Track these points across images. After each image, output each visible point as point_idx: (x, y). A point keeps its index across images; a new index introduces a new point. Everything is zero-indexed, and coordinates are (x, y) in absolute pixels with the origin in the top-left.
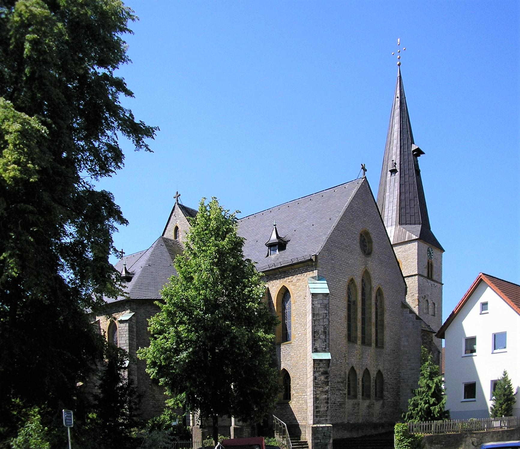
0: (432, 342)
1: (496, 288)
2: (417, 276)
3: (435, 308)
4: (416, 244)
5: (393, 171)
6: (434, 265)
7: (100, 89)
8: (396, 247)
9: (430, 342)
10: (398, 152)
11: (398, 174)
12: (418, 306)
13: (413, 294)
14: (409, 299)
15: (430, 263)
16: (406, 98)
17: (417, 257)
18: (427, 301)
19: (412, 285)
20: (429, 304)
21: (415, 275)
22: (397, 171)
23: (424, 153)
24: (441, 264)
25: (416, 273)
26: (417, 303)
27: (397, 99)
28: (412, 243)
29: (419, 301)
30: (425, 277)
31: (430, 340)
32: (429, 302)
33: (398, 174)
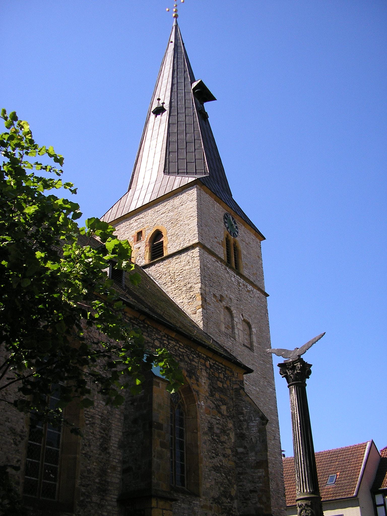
0: (241, 391)
1: (377, 494)
2: (197, 249)
3: (250, 334)
4: (193, 193)
5: (159, 111)
6: (244, 252)
7: (54, 364)
8: (156, 208)
9: (237, 391)
10: (169, 86)
11: (165, 115)
12: (201, 310)
13: (189, 285)
14: (182, 297)
15: (232, 242)
16: (185, 45)
17: (195, 214)
18: (228, 309)
19: (187, 267)
20: (236, 319)
21: (192, 247)
22: (166, 110)
23: (214, 99)
24: (260, 257)
25: (196, 241)
26: (200, 303)
27: (170, 44)
28: (187, 192)
29: (204, 299)
30: (221, 261)
31: (235, 386)
32: (235, 315)
33: (165, 115)
